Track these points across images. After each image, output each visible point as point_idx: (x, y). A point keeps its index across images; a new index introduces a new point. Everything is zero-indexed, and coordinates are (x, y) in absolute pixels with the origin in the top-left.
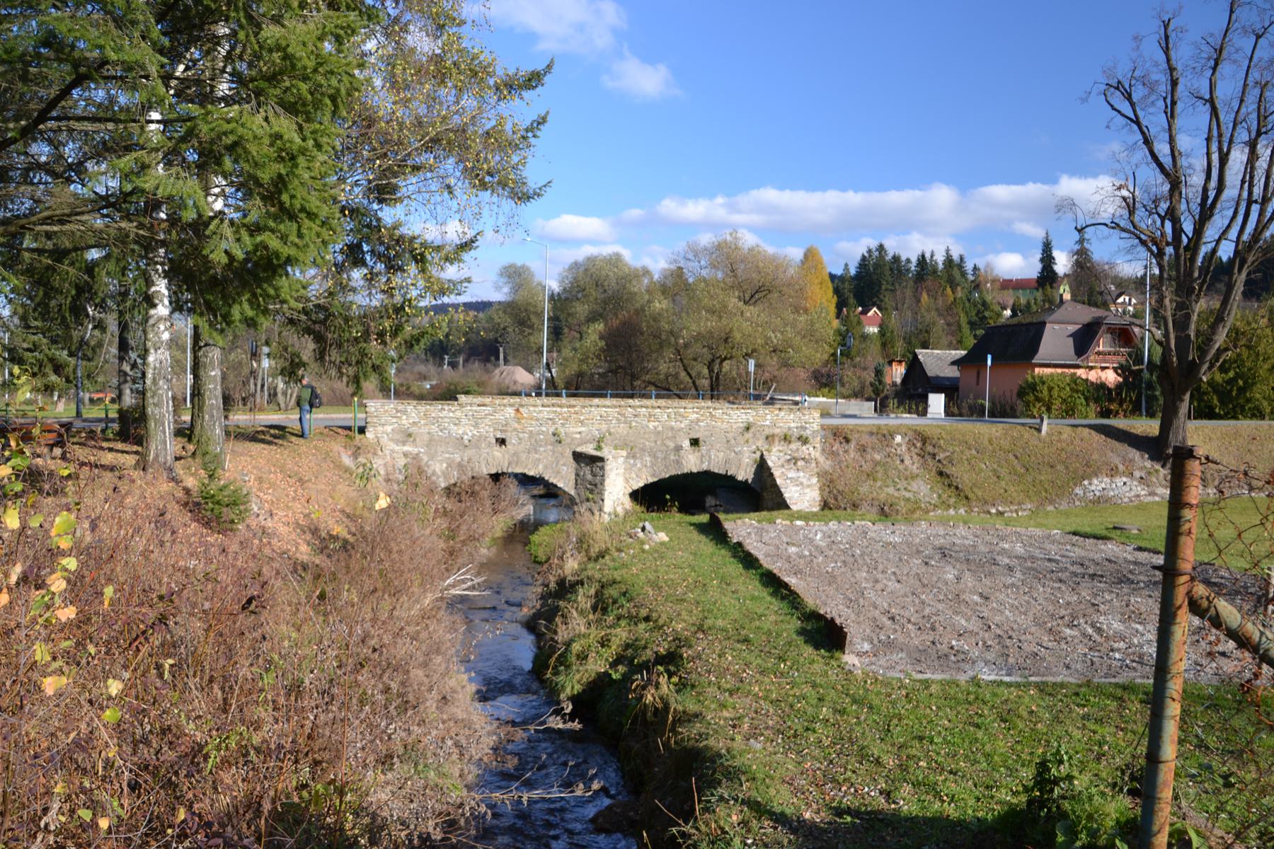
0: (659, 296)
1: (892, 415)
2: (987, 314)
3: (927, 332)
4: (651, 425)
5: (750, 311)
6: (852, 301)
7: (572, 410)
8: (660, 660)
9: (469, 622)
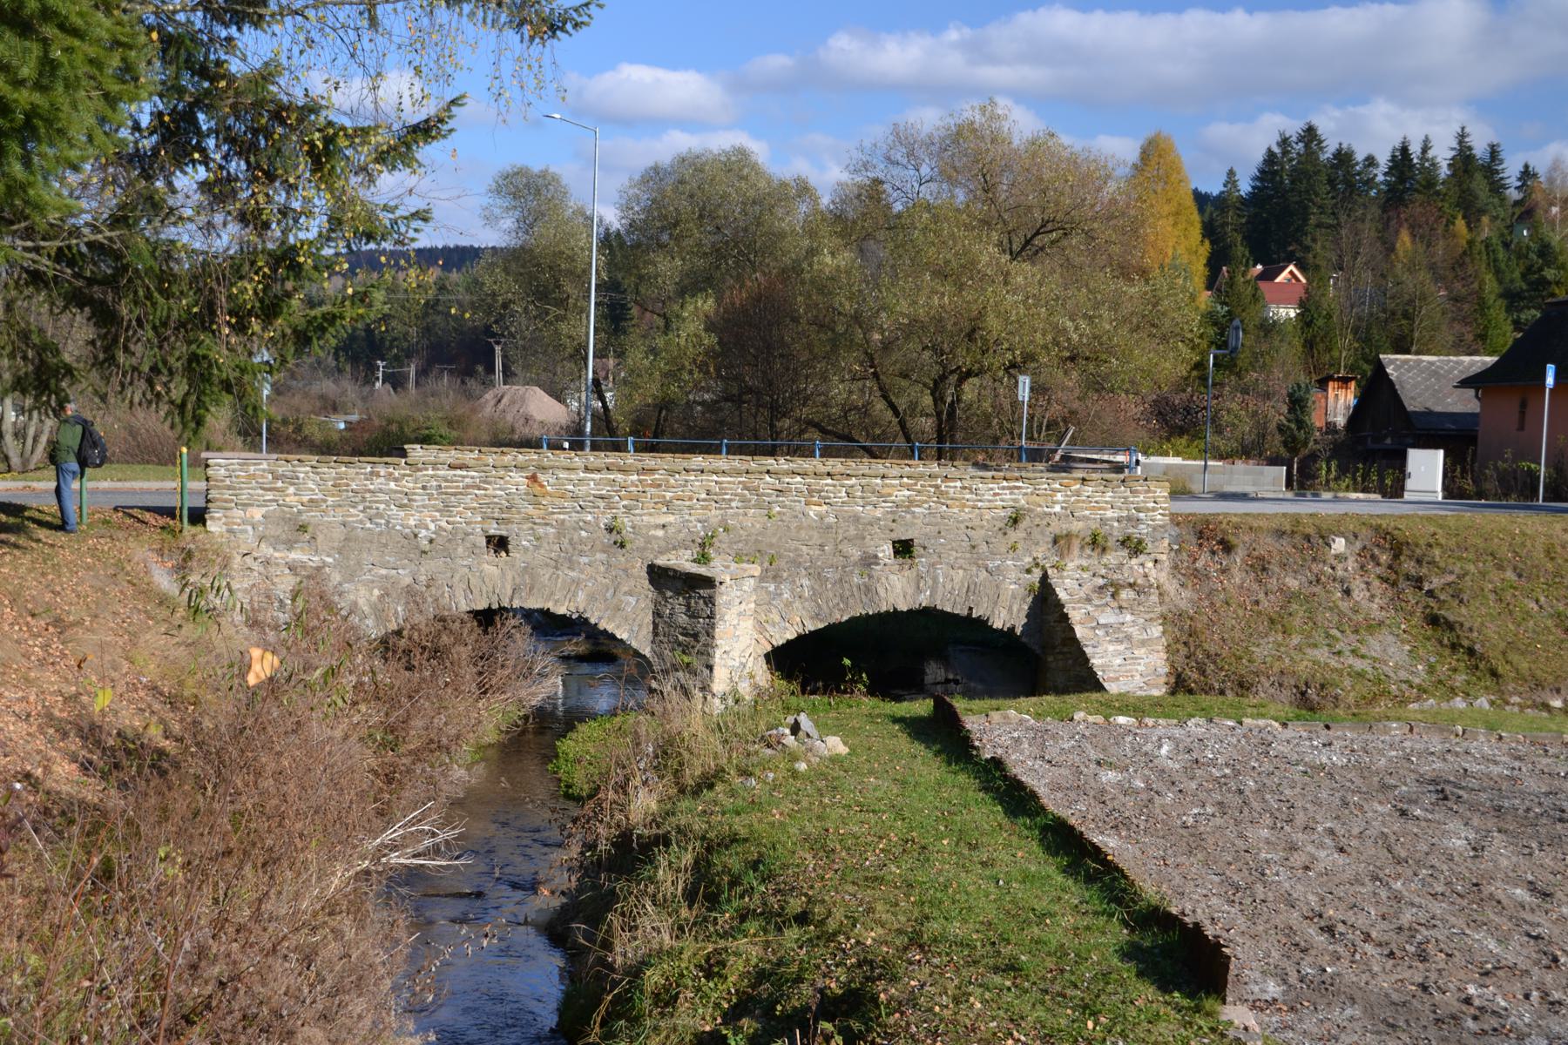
0: (828, 242)
1: (1327, 495)
2: (1550, 274)
3: (1406, 315)
4: (813, 511)
5: (1023, 274)
6: (1241, 250)
7: (648, 478)
8: (831, 1007)
9: (423, 924)
